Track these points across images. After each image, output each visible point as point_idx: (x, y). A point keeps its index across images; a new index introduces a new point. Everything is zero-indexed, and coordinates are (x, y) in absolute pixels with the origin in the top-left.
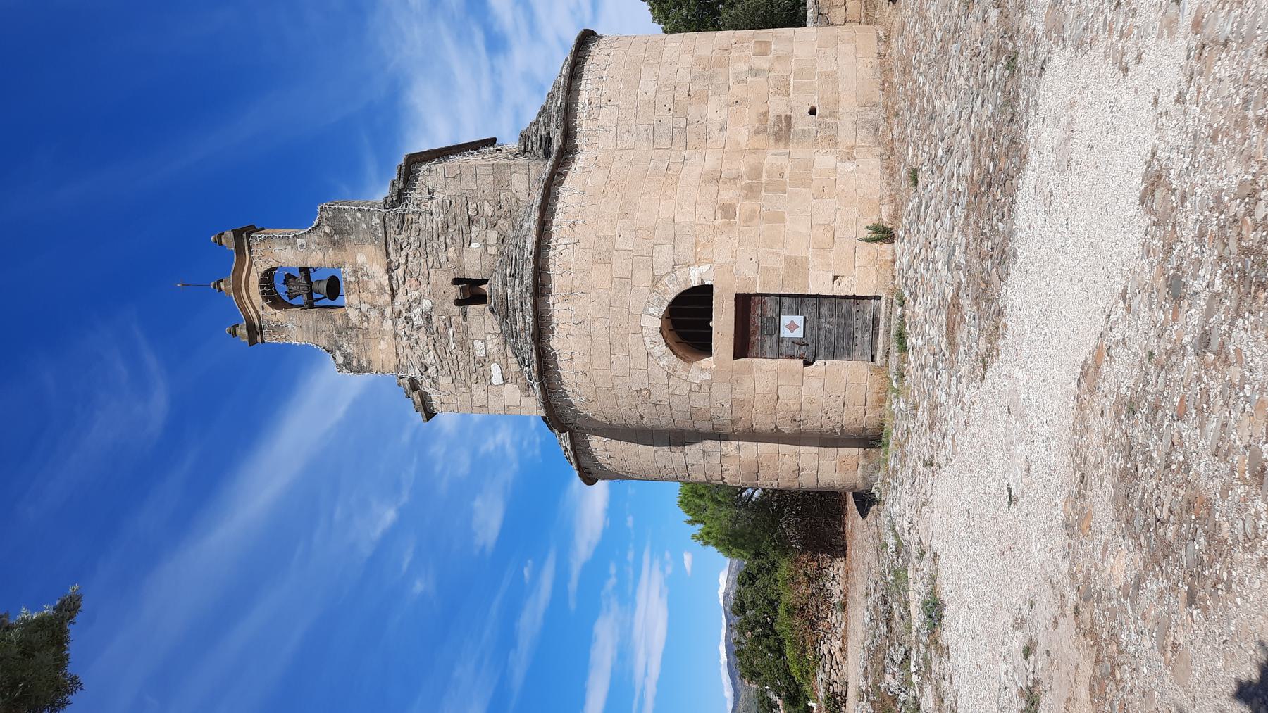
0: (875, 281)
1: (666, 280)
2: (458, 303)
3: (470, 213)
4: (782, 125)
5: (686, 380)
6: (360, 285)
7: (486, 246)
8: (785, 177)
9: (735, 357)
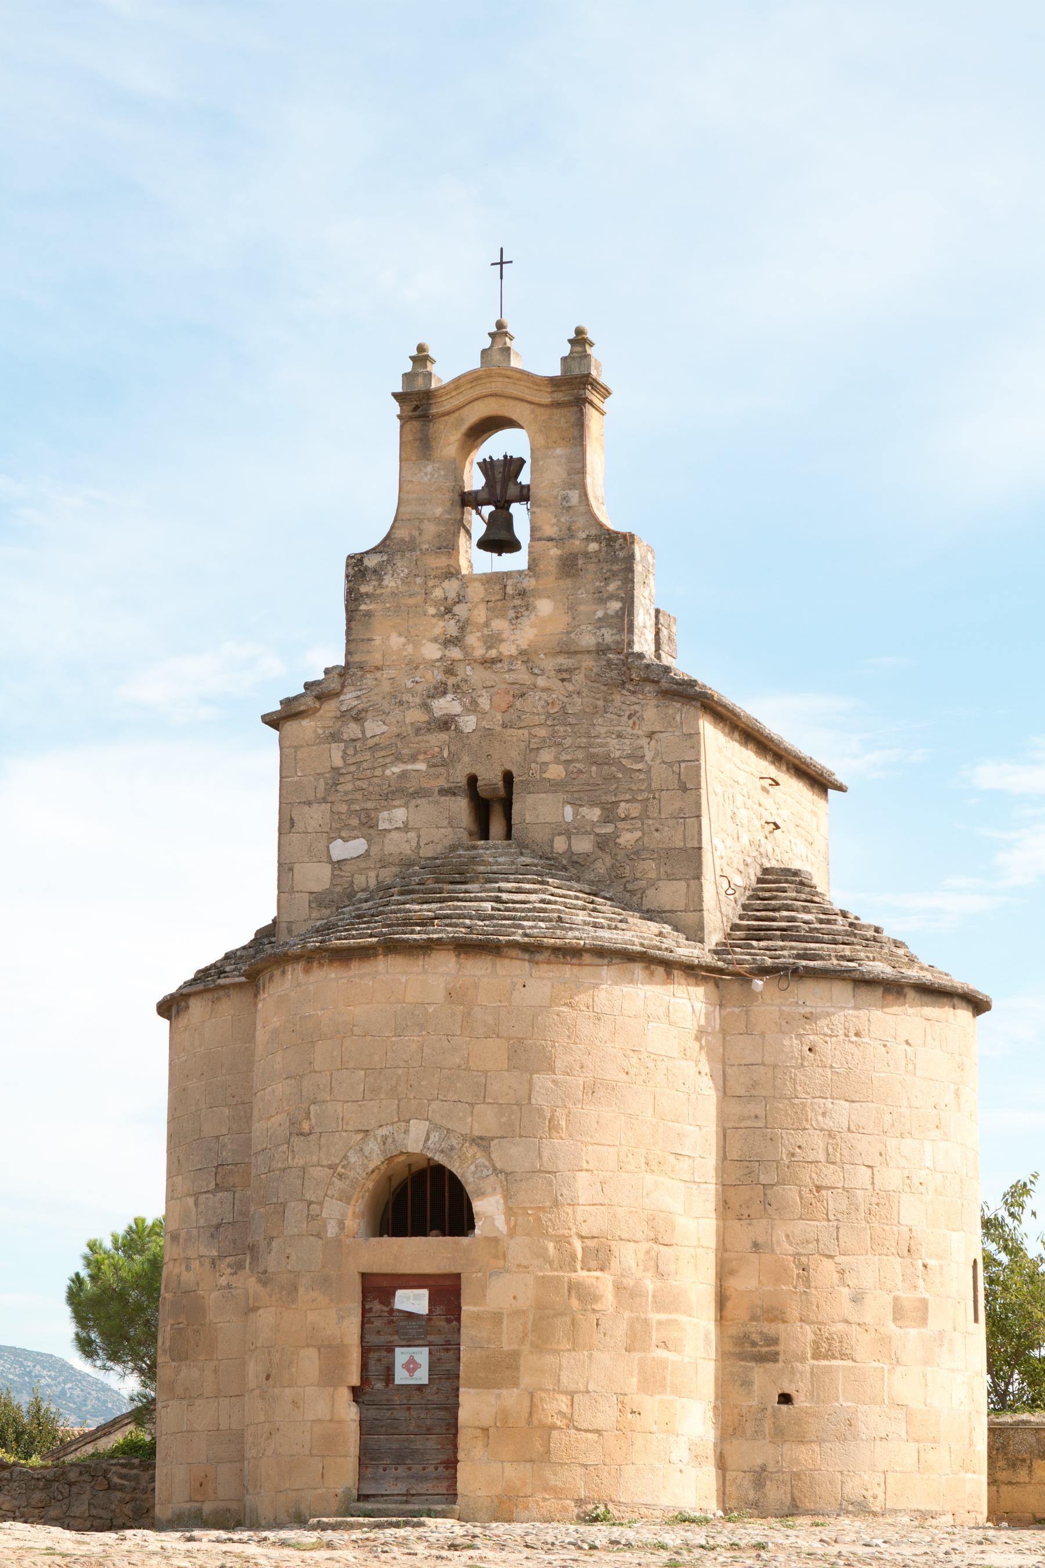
0: (479, 1493)
1: (482, 1160)
2: (473, 780)
3: (623, 804)
4: (762, 1346)
5: (326, 1195)
6: (500, 604)
7: (568, 834)
9: (364, 1276)
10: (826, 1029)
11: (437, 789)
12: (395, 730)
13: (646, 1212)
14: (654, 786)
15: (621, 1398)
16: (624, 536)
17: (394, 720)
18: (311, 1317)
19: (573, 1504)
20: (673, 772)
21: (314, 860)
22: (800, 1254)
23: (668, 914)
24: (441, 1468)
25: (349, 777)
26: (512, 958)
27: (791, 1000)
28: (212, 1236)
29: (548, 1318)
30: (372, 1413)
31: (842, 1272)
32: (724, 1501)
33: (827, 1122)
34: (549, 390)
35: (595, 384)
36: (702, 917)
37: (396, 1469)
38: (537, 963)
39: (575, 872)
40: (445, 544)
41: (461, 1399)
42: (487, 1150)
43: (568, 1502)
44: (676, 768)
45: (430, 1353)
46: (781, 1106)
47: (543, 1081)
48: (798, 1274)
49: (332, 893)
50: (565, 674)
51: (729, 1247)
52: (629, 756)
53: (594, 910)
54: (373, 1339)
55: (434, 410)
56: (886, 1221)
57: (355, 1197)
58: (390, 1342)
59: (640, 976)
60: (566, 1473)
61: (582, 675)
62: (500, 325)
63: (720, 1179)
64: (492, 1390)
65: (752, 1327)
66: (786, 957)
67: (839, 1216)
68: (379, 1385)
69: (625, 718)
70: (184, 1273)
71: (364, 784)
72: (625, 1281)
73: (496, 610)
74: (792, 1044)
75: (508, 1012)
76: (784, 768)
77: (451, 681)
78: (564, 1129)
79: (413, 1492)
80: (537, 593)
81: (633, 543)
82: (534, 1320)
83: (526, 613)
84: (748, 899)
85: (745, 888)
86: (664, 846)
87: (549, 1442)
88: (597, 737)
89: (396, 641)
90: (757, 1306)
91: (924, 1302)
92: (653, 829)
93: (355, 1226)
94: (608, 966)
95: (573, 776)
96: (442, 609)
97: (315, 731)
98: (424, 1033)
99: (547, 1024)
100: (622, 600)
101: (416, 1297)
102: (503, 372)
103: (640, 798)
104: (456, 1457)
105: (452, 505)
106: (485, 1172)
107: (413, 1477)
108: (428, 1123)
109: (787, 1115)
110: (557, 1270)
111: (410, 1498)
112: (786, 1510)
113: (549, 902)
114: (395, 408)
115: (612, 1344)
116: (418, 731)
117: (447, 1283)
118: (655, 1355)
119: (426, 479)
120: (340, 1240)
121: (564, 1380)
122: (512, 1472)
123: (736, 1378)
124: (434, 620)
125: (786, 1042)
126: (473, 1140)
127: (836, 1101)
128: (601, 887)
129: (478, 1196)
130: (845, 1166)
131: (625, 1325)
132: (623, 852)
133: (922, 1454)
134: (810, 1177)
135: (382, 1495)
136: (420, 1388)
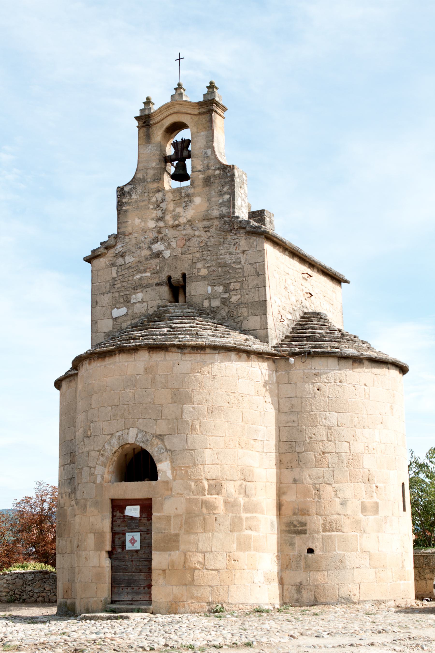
0: (161, 600)
1: (161, 445)
3: (232, 284)
4: (298, 527)
5: (97, 464)
6: (179, 201)
7: (209, 299)
8: (246, 531)
9: (113, 500)
10: (325, 380)
11: (155, 283)
12: (137, 259)
13: (239, 467)
14: (245, 275)
15: (228, 554)
16: (230, 166)
17: (137, 255)
18: (92, 519)
19: (206, 604)
20: (253, 268)
21: (106, 318)
22: (315, 484)
23: (252, 331)
24: (146, 589)
25: (119, 281)
26: (173, 352)
27: (309, 367)
28: (69, 483)
29: (192, 517)
30: (117, 563)
31: (336, 491)
32: (283, 599)
33: (327, 422)
34: (198, 108)
35: (217, 104)
36: (267, 331)
37: (127, 589)
38: (184, 354)
39: (213, 315)
40: (157, 178)
41: (153, 556)
42: (163, 441)
43: (204, 603)
44: (254, 266)
45: (141, 535)
46: (305, 416)
47: (187, 408)
48: (315, 493)
49: (113, 332)
50: (206, 229)
51: (282, 481)
52: (234, 262)
53: (216, 330)
54: (117, 529)
55: (151, 122)
56: (357, 467)
57: (108, 464)
58: (124, 530)
59: (234, 358)
60: (202, 590)
61: (214, 229)
62: (179, 85)
63: (278, 450)
64: (167, 552)
65: (294, 518)
66: (307, 348)
67: (334, 465)
68: (120, 550)
69: (232, 246)
70: (61, 499)
71: (125, 284)
72: (229, 499)
73: (177, 204)
74: (309, 387)
75: (172, 377)
76: (316, 271)
77: (160, 236)
78: (198, 430)
79: (134, 599)
80: (194, 195)
81: (233, 169)
82: (185, 519)
83: (190, 204)
84: (295, 325)
85: (294, 321)
86: (250, 301)
87: (194, 576)
88: (221, 255)
89: (137, 221)
90: (296, 508)
91: (377, 504)
92: (245, 293)
93: (110, 477)
94: (218, 354)
95: (211, 273)
96: (156, 205)
97: (105, 263)
98: (135, 388)
99: (189, 382)
100: (230, 194)
101: (135, 510)
102: (179, 102)
103: (239, 280)
104: (151, 583)
105: (159, 161)
106: (162, 451)
107: (134, 592)
108: (137, 429)
109: (308, 420)
110: (196, 495)
111: (133, 602)
112: (312, 603)
113: (194, 327)
114: (136, 123)
115: (223, 529)
116: (147, 259)
117: (147, 502)
118: (244, 533)
119: (149, 151)
120: (102, 484)
121: (200, 546)
122: (177, 590)
123: (287, 542)
124: (152, 211)
125: (307, 386)
126: (157, 436)
127: (331, 413)
128: (224, 321)
129: (159, 462)
130: (336, 442)
131: (229, 520)
132: (233, 305)
133: (378, 574)
134: (320, 448)
135: (122, 601)
136: (137, 551)
